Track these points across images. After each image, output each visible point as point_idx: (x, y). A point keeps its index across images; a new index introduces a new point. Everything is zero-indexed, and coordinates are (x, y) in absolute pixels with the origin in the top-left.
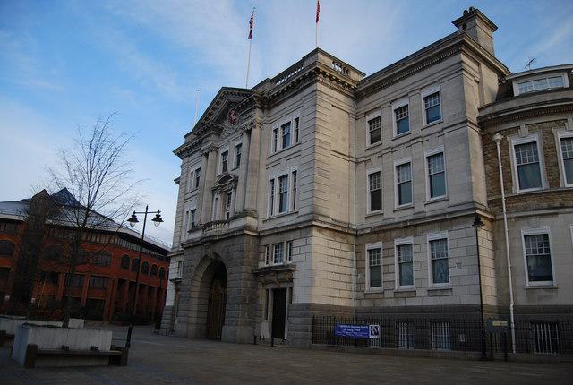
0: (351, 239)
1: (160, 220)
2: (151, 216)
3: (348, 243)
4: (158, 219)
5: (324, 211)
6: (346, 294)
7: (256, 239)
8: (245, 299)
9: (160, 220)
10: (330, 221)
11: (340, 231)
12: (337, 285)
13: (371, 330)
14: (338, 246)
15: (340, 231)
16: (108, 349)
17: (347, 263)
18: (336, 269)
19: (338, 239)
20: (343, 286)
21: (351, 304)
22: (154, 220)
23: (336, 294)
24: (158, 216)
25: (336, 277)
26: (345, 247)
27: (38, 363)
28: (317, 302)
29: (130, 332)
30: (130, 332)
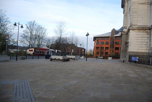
0: (148, 31)
1: (23, 27)
2: (20, 26)
3: (146, 32)
4: (22, 27)
5: (134, 24)
6: (145, 48)
7: (126, 35)
8: (123, 51)
9: (23, 27)
10: (137, 26)
11: (142, 29)
12: (141, 46)
13: (137, 59)
14: (141, 34)
15: (142, 29)
16: (62, 59)
17: (146, 39)
18: (140, 41)
19: (141, 31)
20: (144, 46)
21: (147, 51)
22: (21, 27)
23: (141, 48)
24: (22, 26)
25: (141, 43)
26: (145, 34)
27: (53, 60)
28: (132, 51)
29: (86, 58)
30: (86, 58)
